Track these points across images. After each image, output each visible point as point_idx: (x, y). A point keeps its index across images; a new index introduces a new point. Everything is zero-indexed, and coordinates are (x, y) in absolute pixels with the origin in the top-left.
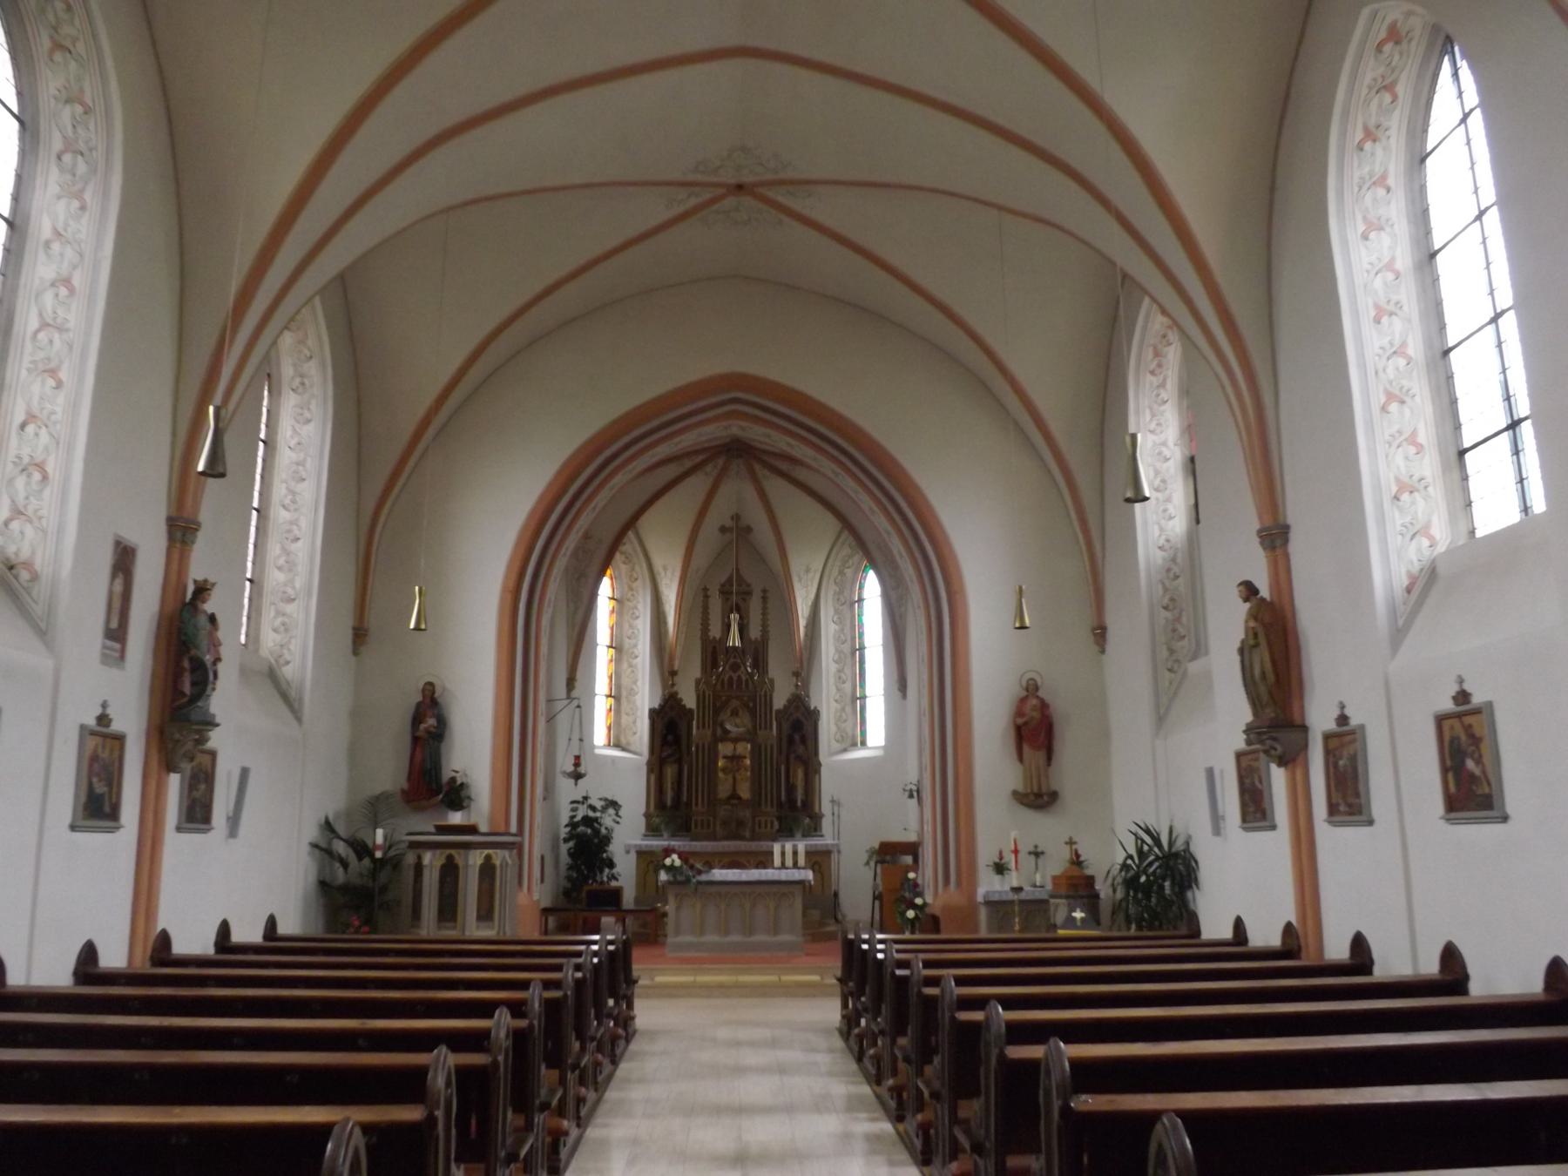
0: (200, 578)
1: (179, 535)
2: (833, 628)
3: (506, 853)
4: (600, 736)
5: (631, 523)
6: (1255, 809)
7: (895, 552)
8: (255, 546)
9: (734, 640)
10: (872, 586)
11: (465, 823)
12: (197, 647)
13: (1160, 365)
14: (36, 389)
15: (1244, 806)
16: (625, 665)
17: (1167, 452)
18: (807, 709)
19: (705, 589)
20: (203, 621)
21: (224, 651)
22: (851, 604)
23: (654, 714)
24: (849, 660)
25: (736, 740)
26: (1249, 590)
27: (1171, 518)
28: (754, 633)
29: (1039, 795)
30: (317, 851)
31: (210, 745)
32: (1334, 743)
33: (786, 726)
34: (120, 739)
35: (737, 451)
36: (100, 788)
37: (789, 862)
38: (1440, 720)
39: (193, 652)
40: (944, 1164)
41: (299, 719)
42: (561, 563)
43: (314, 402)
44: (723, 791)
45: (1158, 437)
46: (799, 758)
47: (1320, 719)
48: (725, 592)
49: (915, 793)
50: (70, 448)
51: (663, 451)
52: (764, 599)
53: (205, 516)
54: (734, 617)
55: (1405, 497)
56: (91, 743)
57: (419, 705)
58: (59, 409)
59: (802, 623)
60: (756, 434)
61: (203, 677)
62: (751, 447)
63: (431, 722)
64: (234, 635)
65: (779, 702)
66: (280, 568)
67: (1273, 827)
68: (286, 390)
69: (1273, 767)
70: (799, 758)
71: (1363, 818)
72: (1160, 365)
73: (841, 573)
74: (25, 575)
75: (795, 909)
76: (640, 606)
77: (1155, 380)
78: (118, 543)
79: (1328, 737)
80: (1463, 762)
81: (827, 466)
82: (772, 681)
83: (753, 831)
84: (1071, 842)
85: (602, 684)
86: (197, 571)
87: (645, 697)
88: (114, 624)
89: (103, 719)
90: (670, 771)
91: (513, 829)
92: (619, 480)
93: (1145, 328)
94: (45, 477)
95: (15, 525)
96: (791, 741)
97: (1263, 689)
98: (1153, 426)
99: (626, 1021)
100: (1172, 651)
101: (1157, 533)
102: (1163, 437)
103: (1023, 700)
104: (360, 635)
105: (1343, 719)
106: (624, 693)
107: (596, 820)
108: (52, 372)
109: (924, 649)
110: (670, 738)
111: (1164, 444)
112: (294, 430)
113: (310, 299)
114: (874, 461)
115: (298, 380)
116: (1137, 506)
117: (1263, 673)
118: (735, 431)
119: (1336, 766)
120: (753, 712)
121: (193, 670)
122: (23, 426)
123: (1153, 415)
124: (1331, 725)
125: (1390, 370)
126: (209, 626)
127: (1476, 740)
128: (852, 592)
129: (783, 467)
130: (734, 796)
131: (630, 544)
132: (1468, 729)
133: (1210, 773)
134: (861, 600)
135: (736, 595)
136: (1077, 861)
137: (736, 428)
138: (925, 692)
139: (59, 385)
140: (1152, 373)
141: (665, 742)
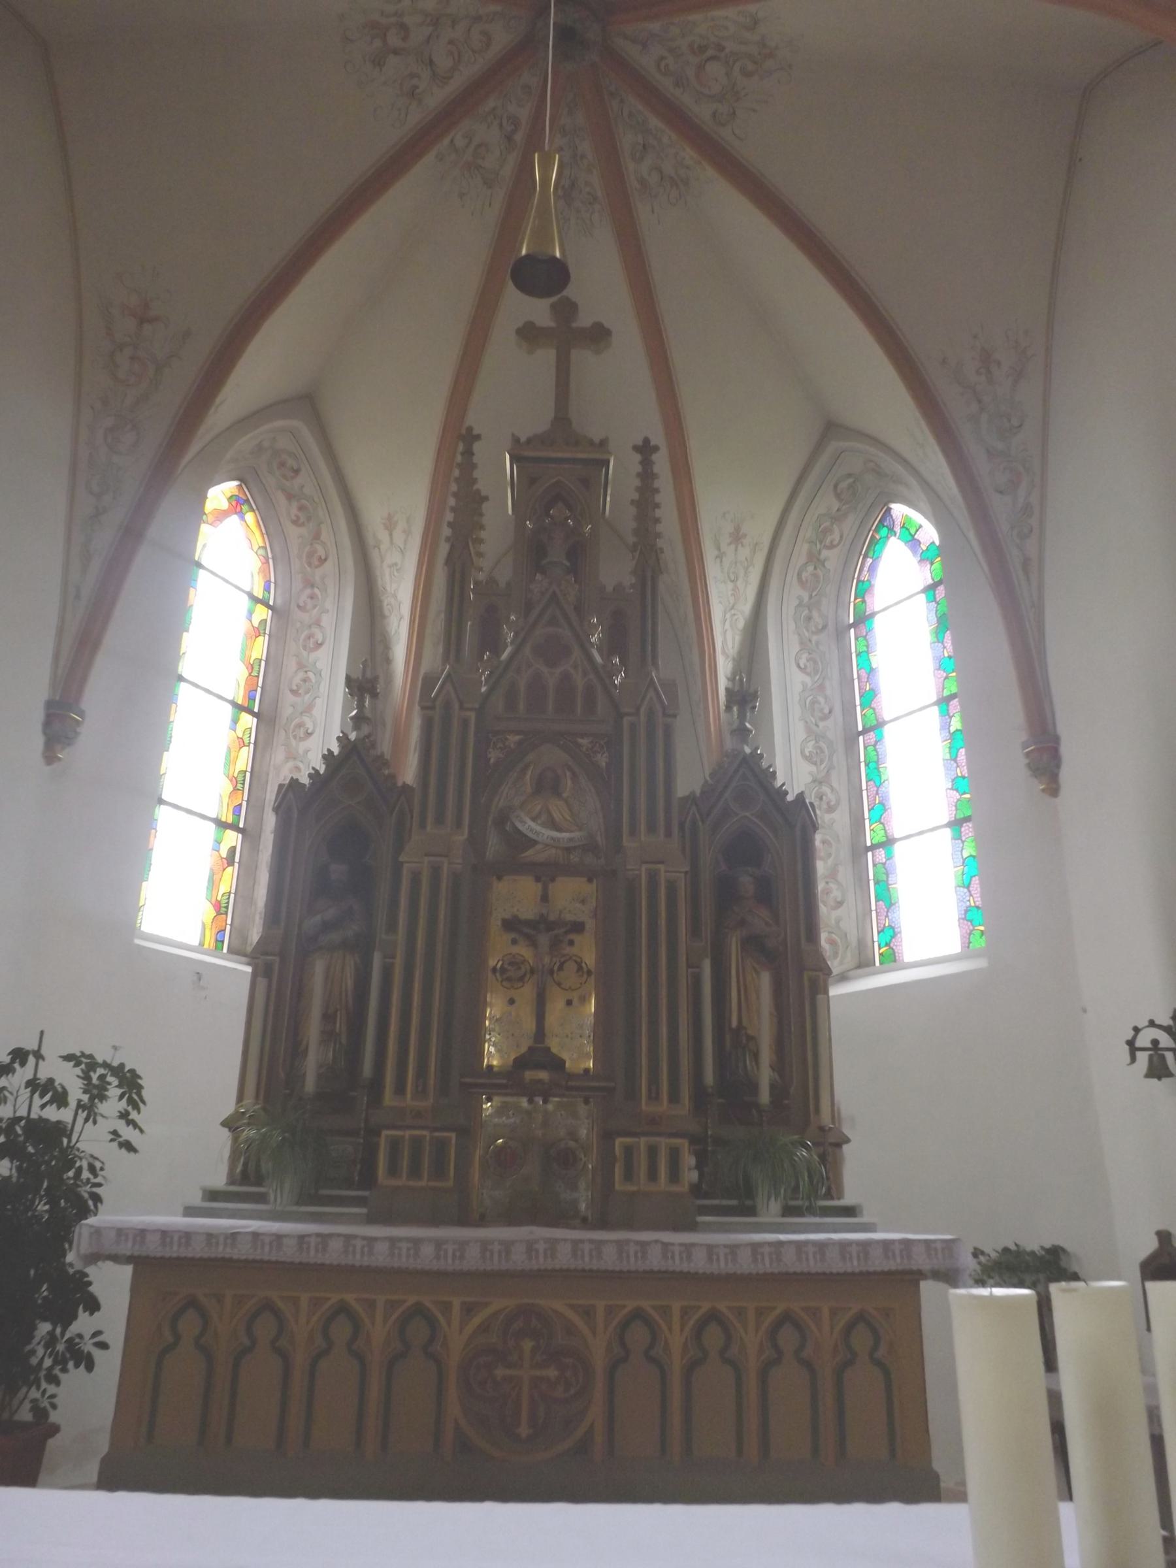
2: (798, 680)
22: (839, 626)
25: (546, 872)
30: (1075, 1268)
46: (755, 945)
59: (724, 668)
70: (755, 945)
73: (814, 559)
76: (327, 621)
107: (60, 1130)
128: (840, 602)
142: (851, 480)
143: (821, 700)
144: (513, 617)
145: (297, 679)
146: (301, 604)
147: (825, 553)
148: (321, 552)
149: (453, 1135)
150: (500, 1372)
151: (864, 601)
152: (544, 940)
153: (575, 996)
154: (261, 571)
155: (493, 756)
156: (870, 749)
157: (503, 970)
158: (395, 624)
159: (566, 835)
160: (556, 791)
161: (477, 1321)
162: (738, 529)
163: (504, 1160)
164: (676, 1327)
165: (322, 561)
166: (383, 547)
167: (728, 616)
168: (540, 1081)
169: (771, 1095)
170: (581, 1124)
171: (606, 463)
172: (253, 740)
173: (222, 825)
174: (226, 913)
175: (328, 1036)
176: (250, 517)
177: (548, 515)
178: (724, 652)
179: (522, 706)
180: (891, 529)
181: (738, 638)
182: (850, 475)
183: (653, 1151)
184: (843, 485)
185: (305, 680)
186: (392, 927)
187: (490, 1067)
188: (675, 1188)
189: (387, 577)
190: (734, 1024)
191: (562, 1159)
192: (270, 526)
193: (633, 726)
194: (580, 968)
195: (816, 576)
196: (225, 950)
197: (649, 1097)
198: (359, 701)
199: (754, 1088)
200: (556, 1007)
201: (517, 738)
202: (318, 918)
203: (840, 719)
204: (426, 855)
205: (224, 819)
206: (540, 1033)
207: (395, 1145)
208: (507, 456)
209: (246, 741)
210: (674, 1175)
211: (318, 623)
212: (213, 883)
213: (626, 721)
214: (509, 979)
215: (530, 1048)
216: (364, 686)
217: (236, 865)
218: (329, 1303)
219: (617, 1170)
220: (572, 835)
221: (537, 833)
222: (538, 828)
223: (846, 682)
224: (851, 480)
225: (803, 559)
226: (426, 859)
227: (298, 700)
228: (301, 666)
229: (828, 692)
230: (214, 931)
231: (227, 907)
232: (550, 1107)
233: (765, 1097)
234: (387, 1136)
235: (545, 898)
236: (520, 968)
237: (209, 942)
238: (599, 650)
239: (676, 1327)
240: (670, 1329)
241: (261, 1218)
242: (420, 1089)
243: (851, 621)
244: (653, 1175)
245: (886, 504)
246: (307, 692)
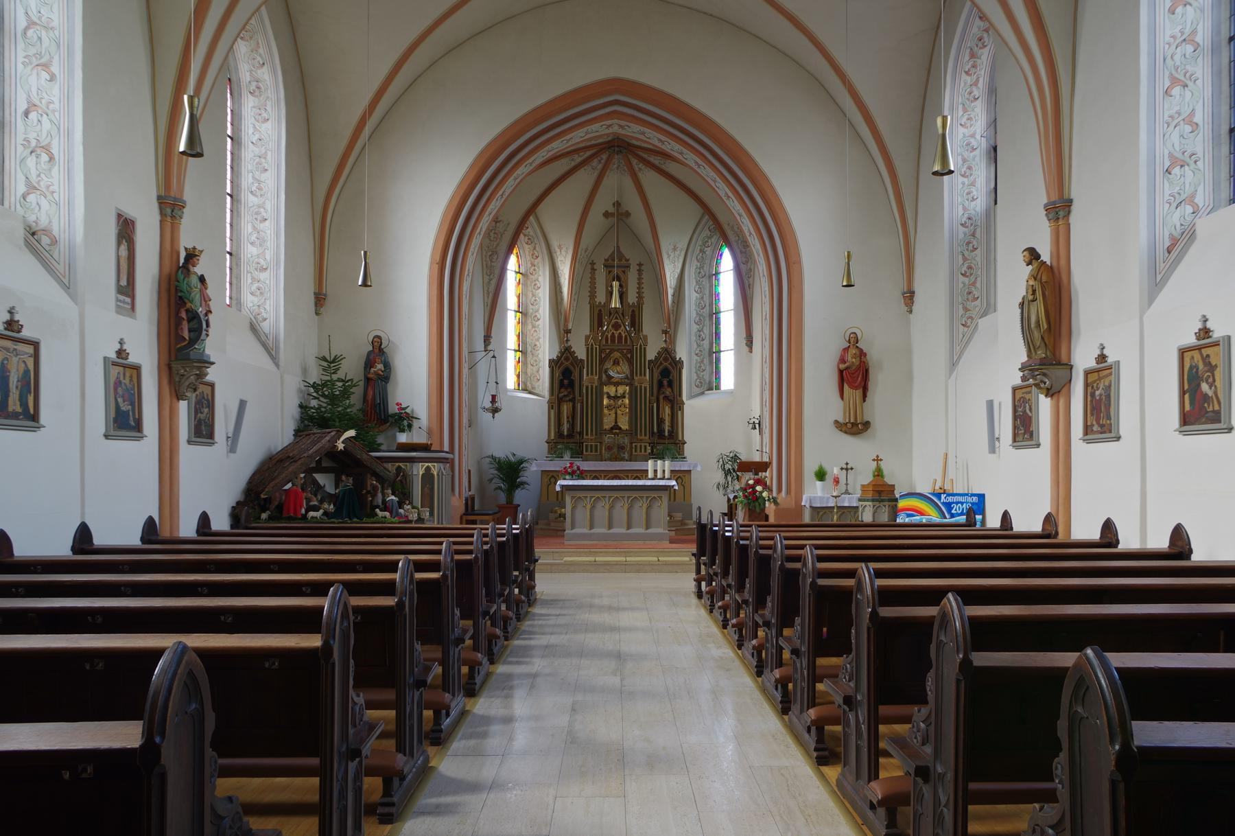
0: (190, 246)
1: (169, 211)
2: (695, 295)
3: (442, 465)
4: (511, 382)
5: (532, 210)
6: (1024, 429)
7: (745, 229)
8: (231, 225)
9: (615, 303)
10: (727, 261)
11: (409, 441)
12: (191, 302)
13: (974, 66)
14: (33, 79)
15: (1015, 427)
16: (530, 327)
17: (974, 143)
18: (674, 359)
19: (593, 264)
20: (194, 280)
21: (213, 305)
23: (553, 363)
24: (707, 322)
25: (617, 384)
26: (1033, 255)
27: (973, 199)
28: (632, 298)
29: (854, 424)
31: (209, 378)
32: (1091, 378)
33: (656, 375)
34: (137, 369)
35: (618, 147)
36: (125, 407)
37: (659, 475)
38: (1182, 352)
39: (189, 305)
40: (802, 711)
41: (277, 365)
42: (476, 242)
43: (269, 103)
44: (608, 423)
45: (964, 127)
46: (666, 398)
47: (1083, 358)
48: (608, 266)
49: (757, 425)
50: (69, 134)
51: (557, 146)
52: (640, 272)
53: (188, 195)
54: (615, 284)
55: (1176, 171)
56: (115, 371)
57: (369, 353)
58: (56, 100)
59: (670, 292)
60: (633, 131)
61: (198, 325)
62: (629, 144)
63: (380, 366)
64: (220, 294)
65: (651, 354)
66: (252, 244)
67: (1038, 445)
68: (245, 92)
69: (1042, 397)
70: (666, 398)
71: (1112, 435)
72: (974, 66)
74: (45, 240)
75: (661, 510)
76: (540, 279)
77: (968, 79)
78: (119, 216)
79: (1087, 373)
80: (1199, 385)
81: (691, 158)
82: (646, 337)
84: (878, 459)
85: (512, 341)
86: (186, 241)
87: (546, 351)
88: (124, 283)
89: (121, 353)
90: (566, 408)
91: (446, 448)
92: (522, 170)
93: (964, 30)
94: (51, 158)
95: (32, 198)
96: (660, 385)
97: (1036, 335)
98: (964, 120)
99: (528, 589)
100: (966, 309)
101: (961, 212)
102: (972, 130)
103: (846, 350)
104: (320, 299)
105: (1102, 358)
106: (529, 349)
108: (46, 66)
109: (767, 308)
110: (566, 382)
111: (973, 136)
112: (254, 127)
113: (258, 9)
114: (716, 140)
115: (254, 84)
116: (945, 177)
117: (1038, 322)
118: (616, 129)
119: (1093, 395)
120: (630, 361)
121: (189, 321)
122: (26, 114)
123: (965, 110)
124: (1092, 364)
125: (1177, 58)
126: (199, 285)
127: (1212, 368)
129: (654, 159)
130: (616, 427)
131: (531, 228)
132: (1206, 359)
133: (990, 404)
134: (717, 274)
135: (617, 268)
136: (879, 473)
137: (615, 127)
138: (767, 344)
139: (52, 78)
140: (967, 73)
141: (562, 385)
163: (609, 448)
191: (621, 448)
223: (711, 295)
240: (921, 513)
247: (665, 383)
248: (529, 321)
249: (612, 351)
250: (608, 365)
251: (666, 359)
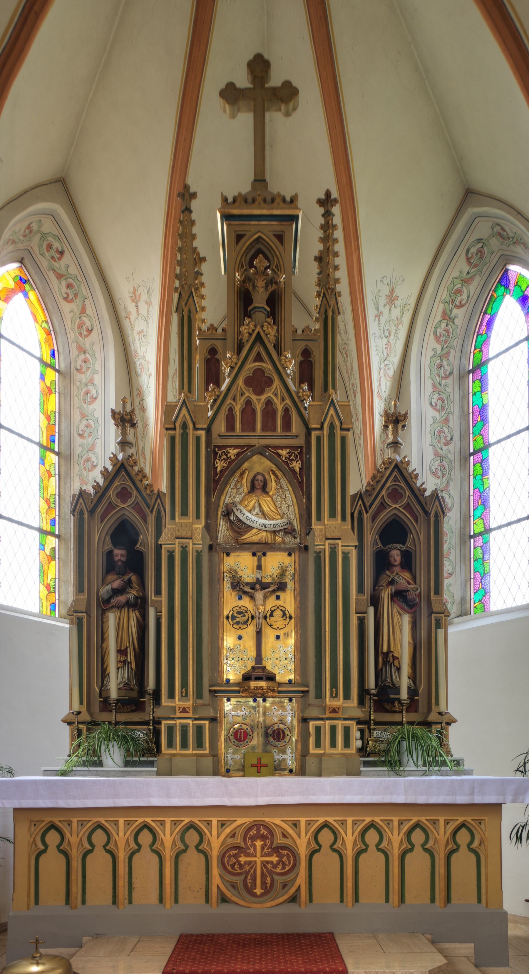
2: (430, 413)
18: (417, 494)
24: (456, 473)
25: (260, 549)
70: (400, 596)
83: (304, 754)
90: (117, 625)
96: (382, 562)
110: (119, 554)
120: (301, 483)
142: (480, 245)
143: (446, 430)
144: (229, 355)
145: (82, 427)
146: (79, 367)
147: (455, 311)
148: (88, 324)
149: (207, 722)
150: (243, 859)
151: (481, 351)
152: (259, 595)
153: (281, 633)
154: (46, 341)
155: (220, 465)
156: (478, 465)
157: (233, 617)
158: (146, 380)
159: (272, 522)
160: (264, 489)
161: (228, 830)
162: (392, 291)
163: (240, 737)
164: (349, 831)
165: (90, 331)
166: (133, 317)
167: (382, 366)
168: (261, 688)
169: (409, 693)
170: (286, 713)
171: (295, 218)
172: (57, 473)
173: (42, 532)
174: (55, 592)
175: (123, 663)
176: (32, 295)
177: (251, 266)
178: (379, 395)
179: (238, 425)
180: (507, 286)
181: (389, 384)
182: (479, 240)
183: (333, 729)
184: (473, 250)
185: (87, 426)
186: (158, 592)
187: (228, 681)
188: (347, 751)
189: (137, 344)
190: (385, 649)
191: (275, 735)
192: (47, 302)
193: (318, 439)
194: (284, 614)
195: (447, 331)
196: (57, 616)
197: (332, 696)
198: (122, 430)
199: (397, 690)
200: (269, 636)
201: (236, 451)
202: (109, 587)
203: (458, 444)
204: (177, 538)
205: (44, 529)
206: (259, 657)
207: (171, 730)
208: (219, 215)
209: (53, 473)
210: (347, 744)
211: (91, 382)
212: (43, 572)
213: (314, 434)
214: (238, 623)
215: (253, 668)
216: (125, 419)
217: (57, 560)
218: (137, 823)
219: (311, 739)
220: (278, 522)
221: (253, 521)
222: (253, 518)
224: (480, 245)
225: (439, 317)
226: (177, 541)
227: (84, 441)
228: (83, 416)
229: (451, 424)
230: (48, 604)
231: (54, 588)
232: (268, 704)
233: (404, 695)
234: (165, 724)
235: (259, 567)
236: (244, 616)
237: (46, 610)
238: (293, 380)
239: (349, 831)
241: (91, 775)
242: (184, 694)
243: (471, 368)
244: (333, 744)
245: (505, 265)
246: (90, 435)
247: (396, 555)
248: (76, 469)
249: (246, 452)
250: (233, 493)
251: (395, 495)
